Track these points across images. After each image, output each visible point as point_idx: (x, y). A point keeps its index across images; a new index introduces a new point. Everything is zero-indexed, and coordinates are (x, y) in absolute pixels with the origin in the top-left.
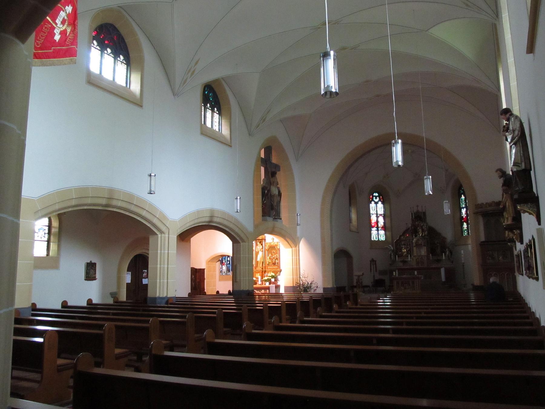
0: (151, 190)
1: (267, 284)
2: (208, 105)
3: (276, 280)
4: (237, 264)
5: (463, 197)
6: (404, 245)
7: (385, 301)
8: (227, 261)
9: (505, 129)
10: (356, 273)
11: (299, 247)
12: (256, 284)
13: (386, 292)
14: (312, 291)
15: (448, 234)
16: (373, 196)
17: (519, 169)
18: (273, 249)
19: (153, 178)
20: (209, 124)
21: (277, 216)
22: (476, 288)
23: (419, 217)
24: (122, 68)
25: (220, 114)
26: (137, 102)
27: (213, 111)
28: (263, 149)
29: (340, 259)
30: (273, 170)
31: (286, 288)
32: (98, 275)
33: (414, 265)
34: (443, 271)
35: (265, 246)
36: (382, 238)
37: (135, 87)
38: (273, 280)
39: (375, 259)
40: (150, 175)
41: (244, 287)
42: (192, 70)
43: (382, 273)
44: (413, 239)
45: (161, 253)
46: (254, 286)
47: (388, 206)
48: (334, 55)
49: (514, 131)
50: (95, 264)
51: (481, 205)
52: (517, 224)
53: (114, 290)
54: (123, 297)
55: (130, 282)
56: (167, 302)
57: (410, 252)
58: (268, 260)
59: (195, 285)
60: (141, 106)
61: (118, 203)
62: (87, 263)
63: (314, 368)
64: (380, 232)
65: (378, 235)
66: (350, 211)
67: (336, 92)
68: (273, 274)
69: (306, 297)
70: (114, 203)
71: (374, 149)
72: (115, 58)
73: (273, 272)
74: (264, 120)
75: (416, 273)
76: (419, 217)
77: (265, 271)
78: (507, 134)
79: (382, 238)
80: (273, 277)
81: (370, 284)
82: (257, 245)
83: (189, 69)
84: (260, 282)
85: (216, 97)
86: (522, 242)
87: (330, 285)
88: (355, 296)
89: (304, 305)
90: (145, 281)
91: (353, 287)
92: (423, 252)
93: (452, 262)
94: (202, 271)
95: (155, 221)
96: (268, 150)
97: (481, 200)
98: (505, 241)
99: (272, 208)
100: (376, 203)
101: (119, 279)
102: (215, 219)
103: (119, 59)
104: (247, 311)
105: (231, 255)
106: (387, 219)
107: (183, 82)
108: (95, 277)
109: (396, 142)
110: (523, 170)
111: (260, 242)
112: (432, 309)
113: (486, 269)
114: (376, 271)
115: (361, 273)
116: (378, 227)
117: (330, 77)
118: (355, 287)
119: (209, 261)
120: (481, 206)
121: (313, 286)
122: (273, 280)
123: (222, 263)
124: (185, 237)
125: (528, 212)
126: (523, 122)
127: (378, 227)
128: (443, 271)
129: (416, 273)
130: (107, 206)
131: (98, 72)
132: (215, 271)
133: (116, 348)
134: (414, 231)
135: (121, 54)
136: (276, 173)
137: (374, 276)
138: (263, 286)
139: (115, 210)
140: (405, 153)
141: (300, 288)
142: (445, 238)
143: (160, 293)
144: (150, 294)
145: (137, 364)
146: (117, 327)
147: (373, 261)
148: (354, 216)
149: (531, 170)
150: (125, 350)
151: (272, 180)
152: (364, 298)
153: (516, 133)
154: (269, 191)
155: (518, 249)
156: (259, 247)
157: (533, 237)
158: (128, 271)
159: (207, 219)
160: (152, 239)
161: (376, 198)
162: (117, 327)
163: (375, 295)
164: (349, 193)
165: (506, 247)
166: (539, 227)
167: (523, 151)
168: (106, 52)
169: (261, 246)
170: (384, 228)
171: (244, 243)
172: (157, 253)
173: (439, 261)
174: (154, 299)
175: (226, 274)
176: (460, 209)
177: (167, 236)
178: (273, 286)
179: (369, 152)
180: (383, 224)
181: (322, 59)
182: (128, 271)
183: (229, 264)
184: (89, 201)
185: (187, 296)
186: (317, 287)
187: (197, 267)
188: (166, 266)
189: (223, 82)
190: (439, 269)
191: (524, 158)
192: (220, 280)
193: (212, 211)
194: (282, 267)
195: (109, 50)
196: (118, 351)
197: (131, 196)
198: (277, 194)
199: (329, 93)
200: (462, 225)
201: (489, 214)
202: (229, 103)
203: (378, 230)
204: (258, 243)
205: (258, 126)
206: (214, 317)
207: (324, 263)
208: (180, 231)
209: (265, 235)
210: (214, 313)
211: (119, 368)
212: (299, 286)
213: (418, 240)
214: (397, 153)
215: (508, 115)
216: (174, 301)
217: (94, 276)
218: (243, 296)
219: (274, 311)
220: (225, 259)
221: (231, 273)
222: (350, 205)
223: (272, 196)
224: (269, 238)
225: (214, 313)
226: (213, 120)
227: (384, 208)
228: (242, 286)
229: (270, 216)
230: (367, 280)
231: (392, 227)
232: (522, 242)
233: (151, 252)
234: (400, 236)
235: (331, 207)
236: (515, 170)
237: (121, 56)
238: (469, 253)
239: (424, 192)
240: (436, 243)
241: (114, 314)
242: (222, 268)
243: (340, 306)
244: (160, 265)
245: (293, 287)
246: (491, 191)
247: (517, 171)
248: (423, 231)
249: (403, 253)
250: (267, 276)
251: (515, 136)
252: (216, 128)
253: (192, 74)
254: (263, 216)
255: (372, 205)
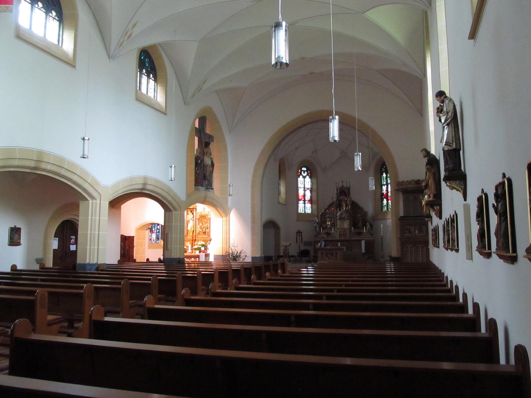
0: (84, 154)
1: (197, 252)
2: (144, 71)
3: (206, 249)
4: (166, 233)
5: (384, 175)
6: (329, 218)
7: (308, 271)
8: (157, 229)
9: (439, 110)
10: (283, 243)
11: (229, 217)
12: (186, 252)
13: (313, 260)
14: (241, 260)
15: (369, 208)
16: (301, 171)
17: (450, 148)
18: (203, 218)
19: (86, 142)
20: (144, 90)
21: (209, 186)
22: (393, 259)
23: (344, 192)
24: (53, 24)
25: (155, 80)
26: (71, 63)
27: (148, 76)
28: (197, 120)
29: (269, 229)
30: (207, 140)
31: (216, 257)
32: (23, 240)
33: (338, 238)
34: (363, 243)
35: (196, 215)
36: (309, 211)
37: (68, 46)
38: (203, 249)
39: (301, 231)
40: (84, 139)
41: (175, 255)
42: (129, 33)
43: (307, 244)
44: (337, 213)
45: (92, 219)
46: (185, 254)
47: (314, 180)
48: (286, 26)
49: (448, 113)
50: (20, 229)
51: (402, 182)
52: (436, 202)
53: (40, 256)
54: (49, 264)
55: (57, 248)
56: (97, 269)
57: (334, 225)
58: (198, 229)
59: (124, 252)
60: (75, 67)
61: (48, 167)
62: (11, 228)
63: (260, 332)
64: (306, 205)
65: (305, 208)
66: (279, 184)
67: (286, 63)
68: (203, 243)
69: (235, 265)
70: (43, 166)
71: (305, 125)
72: (47, 13)
73: (203, 241)
74: (200, 90)
75: (339, 244)
76: (344, 192)
77: (195, 240)
78: (441, 115)
79: (309, 211)
80: (203, 245)
81: (296, 255)
82: (188, 214)
83: (126, 31)
84: (190, 251)
85: (152, 62)
86: (440, 217)
87: (258, 255)
88: (283, 265)
89: (236, 272)
90: (73, 248)
91: (279, 257)
92: (346, 224)
93: (372, 235)
94: (131, 239)
95: (86, 186)
96: (203, 120)
97: (401, 179)
98: (423, 216)
99: (205, 177)
100: (304, 177)
101: (46, 245)
102: (148, 187)
103: (50, 14)
104: (176, 278)
105: (162, 223)
106: (313, 193)
107: (119, 44)
108: (20, 242)
109: (334, 118)
110: (454, 149)
111: (191, 212)
112: (358, 277)
113: (404, 242)
114: (302, 242)
115: (288, 244)
116: (305, 201)
117: (281, 49)
118: (282, 256)
119: (139, 229)
120: (401, 183)
121: (242, 255)
122: (203, 249)
123: (151, 231)
124: (116, 203)
125: (455, 189)
126: (456, 104)
127: (305, 201)
128: (363, 243)
129: (339, 244)
130: (36, 168)
131: (28, 27)
132: (144, 239)
133: (49, 314)
134: (339, 206)
135: (53, 10)
136: (209, 144)
137: (300, 246)
138: (193, 254)
139: (44, 173)
140: (341, 130)
141: (230, 257)
142: (366, 213)
143: (90, 261)
144: (79, 261)
145: (70, 331)
146: (50, 293)
147: (299, 232)
148: (283, 189)
149: (460, 150)
150: (59, 316)
151: (206, 150)
152: (290, 267)
153: (450, 114)
154: (202, 161)
155: (435, 224)
156: (190, 216)
157: (455, 212)
158: (55, 236)
159: (140, 187)
160: (82, 204)
161: (304, 173)
162: (50, 293)
163: (298, 265)
164: (280, 166)
165: (422, 221)
166: (465, 202)
167: (455, 132)
168: (36, 6)
169: (192, 215)
170: (311, 201)
171: (176, 212)
172: (88, 219)
173: (359, 234)
174: (84, 266)
175: (156, 242)
176: (382, 185)
177: (98, 202)
178: (202, 255)
179: (300, 127)
180: (309, 198)
181: (273, 29)
182: (55, 236)
183: (159, 232)
184: (16, 163)
185: (116, 263)
186: (246, 256)
187: (127, 234)
188: (97, 232)
189: (160, 48)
190: (360, 241)
191: (456, 139)
192: (149, 248)
193: (145, 178)
194: (212, 236)
195: (40, 5)
196: (50, 317)
197: (62, 159)
198: (210, 164)
199: (279, 64)
200: (382, 200)
201: (410, 191)
202: (164, 65)
203: (305, 203)
204: (189, 212)
205: (194, 96)
206: (150, 284)
207: (253, 233)
208: (112, 198)
209: (197, 204)
210: (149, 280)
211: (50, 333)
212: (229, 255)
213: (342, 214)
214: (334, 129)
215: (442, 98)
216: (105, 268)
217: (18, 241)
218: (173, 263)
219: (208, 278)
220: (155, 227)
221: (161, 242)
222: (280, 178)
223: (205, 166)
224: (201, 208)
225: (149, 280)
226: (149, 87)
227: (312, 182)
228: (173, 254)
229: (202, 186)
230: (293, 251)
231: (318, 201)
232: (440, 217)
233: (81, 219)
234: (326, 210)
235: (262, 179)
236: (447, 149)
237: (53, 12)
238: (388, 226)
239: (354, 169)
240: (358, 217)
241: (42, 280)
242: (151, 236)
243: (259, 277)
244: (91, 230)
245: (223, 255)
246: (415, 170)
247: (448, 150)
248: (346, 205)
249: (327, 225)
250: (197, 245)
251: (448, 117)
252: (151, 94)
253: (130, 36)
254: (195, 185)
255: (301, 179)
